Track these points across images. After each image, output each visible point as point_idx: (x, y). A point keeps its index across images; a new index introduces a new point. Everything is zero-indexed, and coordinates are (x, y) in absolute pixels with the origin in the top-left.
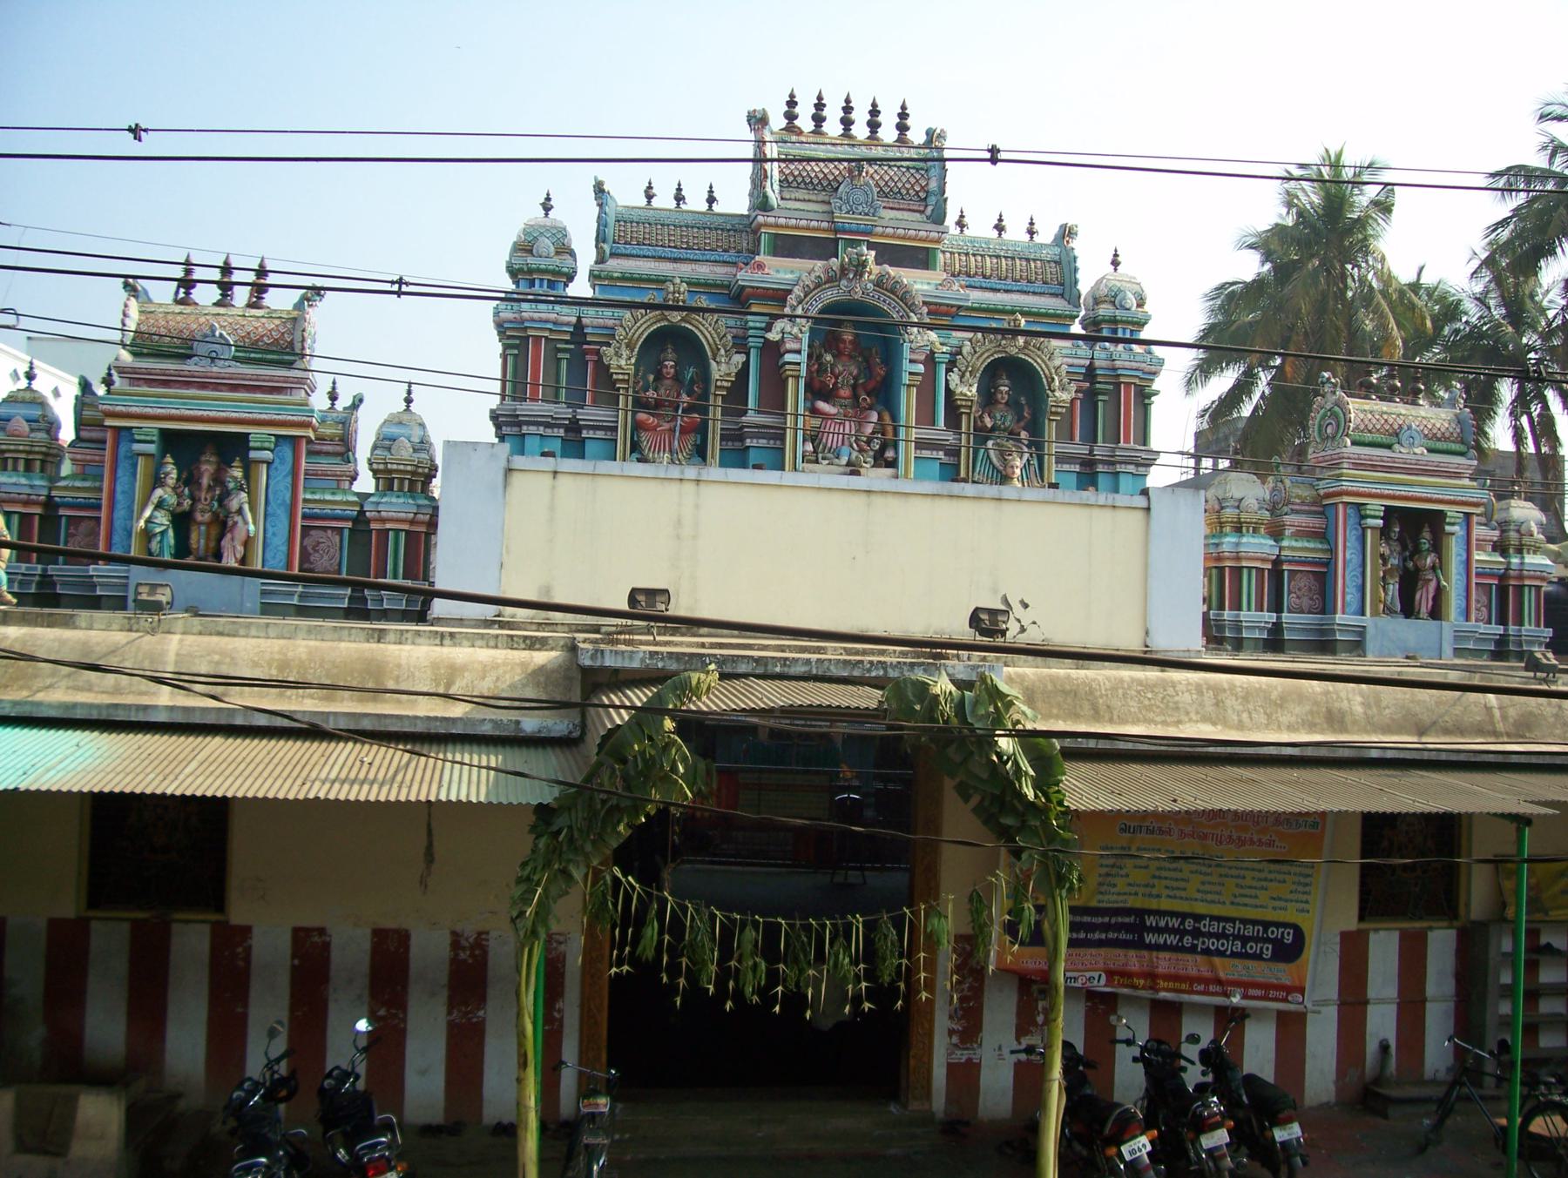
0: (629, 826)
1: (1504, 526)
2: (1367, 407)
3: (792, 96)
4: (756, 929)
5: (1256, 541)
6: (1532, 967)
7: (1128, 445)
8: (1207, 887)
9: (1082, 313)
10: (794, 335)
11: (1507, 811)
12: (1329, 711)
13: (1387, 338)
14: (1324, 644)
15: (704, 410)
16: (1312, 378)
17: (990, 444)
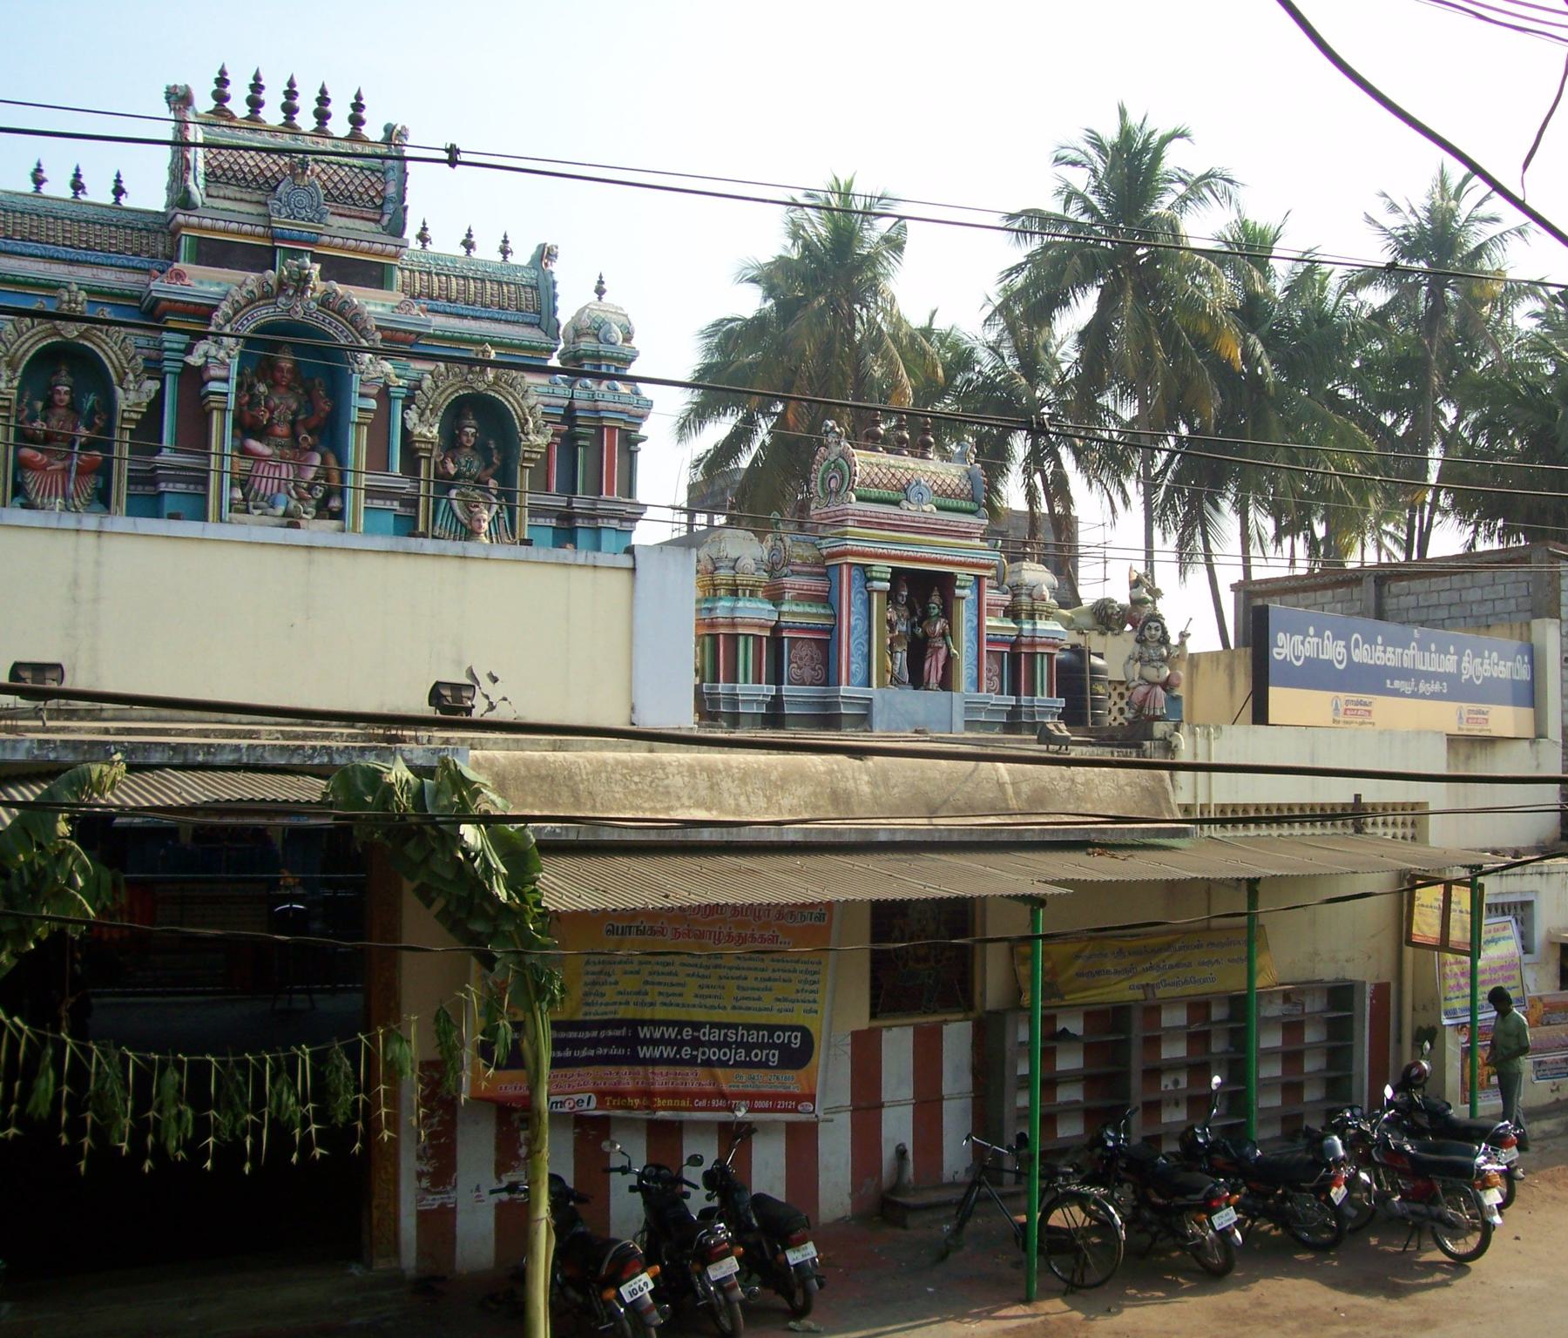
0: (13, 954)
1: (1015, 590)
2: (873, 460)
3: (223, 72)
4: (180, 1070)
5: (754, 605)
6: (1049, 1054)
7: (611, 497)
8: (705, 992)
9: (561, 346)
10: (220, 359)
11: (1021, 893)
12: (834, 792)
13: (896, 385)
14: (829, 720)
15: (107, 447)
16: (816, 426)
17: (453, 493)
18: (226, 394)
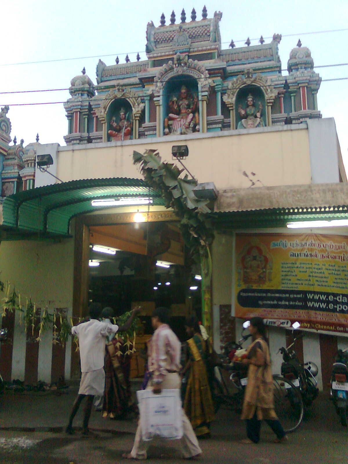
18: (159, 100)
